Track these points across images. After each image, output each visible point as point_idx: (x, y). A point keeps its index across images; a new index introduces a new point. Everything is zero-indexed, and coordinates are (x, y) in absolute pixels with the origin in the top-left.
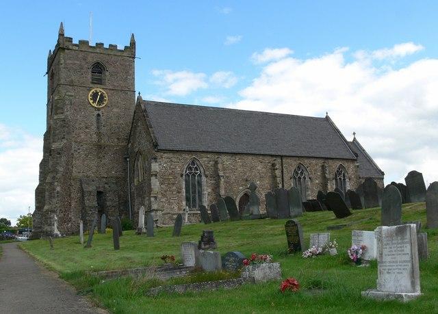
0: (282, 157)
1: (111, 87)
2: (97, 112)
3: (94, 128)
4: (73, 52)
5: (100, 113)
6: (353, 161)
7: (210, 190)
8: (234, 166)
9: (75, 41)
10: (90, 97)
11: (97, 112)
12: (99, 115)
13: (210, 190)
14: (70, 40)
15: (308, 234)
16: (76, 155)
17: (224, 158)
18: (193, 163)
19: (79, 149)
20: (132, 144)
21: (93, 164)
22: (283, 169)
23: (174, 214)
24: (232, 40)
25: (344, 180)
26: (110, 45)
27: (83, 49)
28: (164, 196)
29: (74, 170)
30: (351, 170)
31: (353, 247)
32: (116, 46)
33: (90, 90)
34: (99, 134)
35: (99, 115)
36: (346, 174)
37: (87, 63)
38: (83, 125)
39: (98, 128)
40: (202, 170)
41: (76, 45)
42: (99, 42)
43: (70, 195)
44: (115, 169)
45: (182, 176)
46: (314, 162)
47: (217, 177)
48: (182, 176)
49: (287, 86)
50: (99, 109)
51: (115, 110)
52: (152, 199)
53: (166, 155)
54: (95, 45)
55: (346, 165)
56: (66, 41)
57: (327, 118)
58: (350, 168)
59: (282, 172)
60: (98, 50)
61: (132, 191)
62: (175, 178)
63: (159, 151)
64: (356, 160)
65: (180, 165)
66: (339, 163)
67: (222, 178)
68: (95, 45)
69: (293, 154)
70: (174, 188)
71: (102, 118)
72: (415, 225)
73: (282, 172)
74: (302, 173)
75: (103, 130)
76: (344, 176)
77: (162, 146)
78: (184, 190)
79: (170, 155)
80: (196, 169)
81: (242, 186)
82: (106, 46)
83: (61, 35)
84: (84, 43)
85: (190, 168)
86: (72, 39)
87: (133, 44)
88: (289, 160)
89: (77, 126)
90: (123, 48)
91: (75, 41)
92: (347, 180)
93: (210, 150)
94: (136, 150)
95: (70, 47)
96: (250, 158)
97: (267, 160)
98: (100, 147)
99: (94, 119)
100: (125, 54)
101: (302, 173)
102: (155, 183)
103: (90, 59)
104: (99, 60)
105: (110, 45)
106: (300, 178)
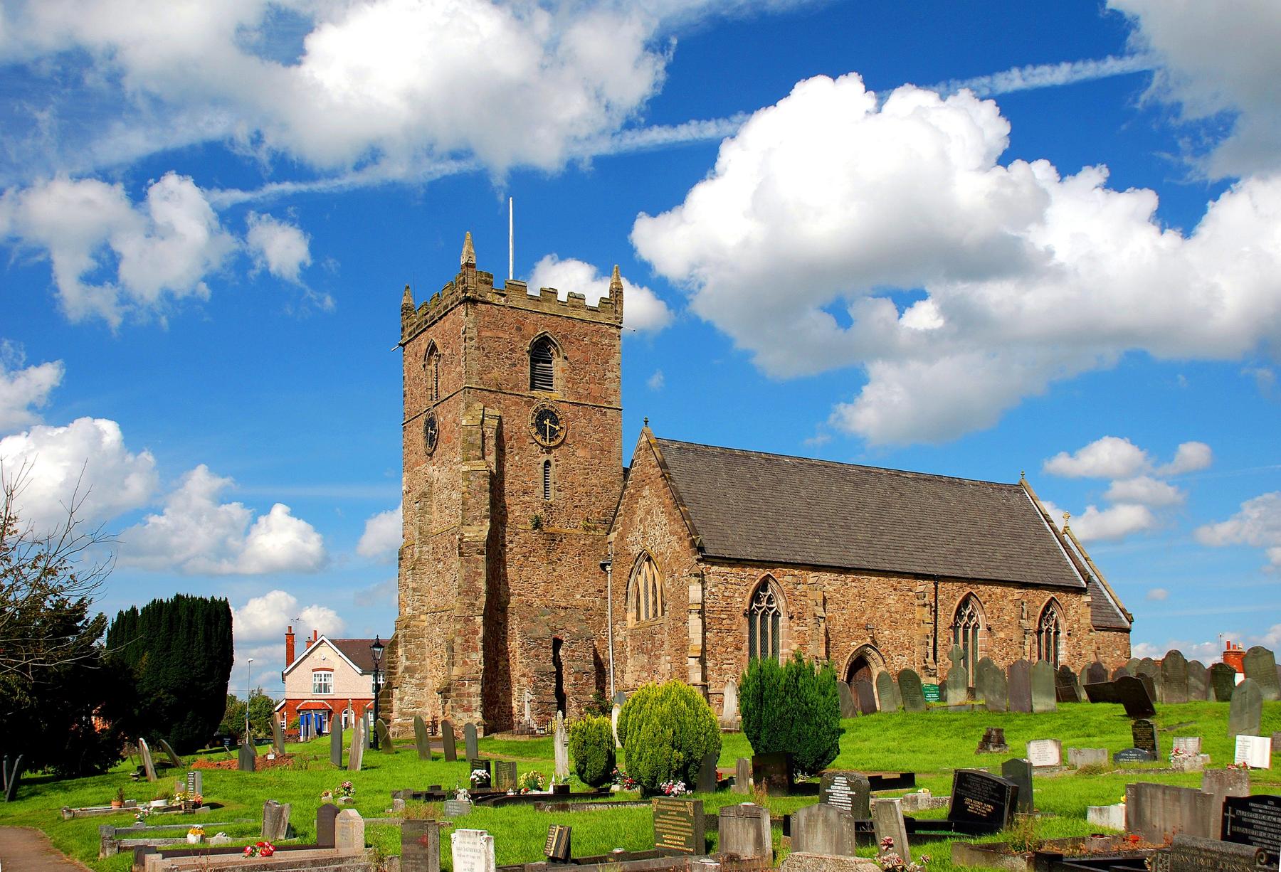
2: (545, 457)
5: (551, 457)
11: (545, 457)
15: (396, 719)
20: (622, 537)
24: (1159, 593)
25: (1057, 633)
27: (514, 304)
31: (800, 775)
35: (547, 463)
42: (547, 287)
49: (1047, 507)
51: (580, 453)
53: (714, 569)
59: (936, 611)
61: (618, 639)
69: (959, 573)
76: (1056, 625)
78: (747, 644)
82: (562, 297)
88: (949, 586)
93: (799, 559)
94: (636, 550)
95: (489, 297)
100: (602, 318)
103: (529, 329)
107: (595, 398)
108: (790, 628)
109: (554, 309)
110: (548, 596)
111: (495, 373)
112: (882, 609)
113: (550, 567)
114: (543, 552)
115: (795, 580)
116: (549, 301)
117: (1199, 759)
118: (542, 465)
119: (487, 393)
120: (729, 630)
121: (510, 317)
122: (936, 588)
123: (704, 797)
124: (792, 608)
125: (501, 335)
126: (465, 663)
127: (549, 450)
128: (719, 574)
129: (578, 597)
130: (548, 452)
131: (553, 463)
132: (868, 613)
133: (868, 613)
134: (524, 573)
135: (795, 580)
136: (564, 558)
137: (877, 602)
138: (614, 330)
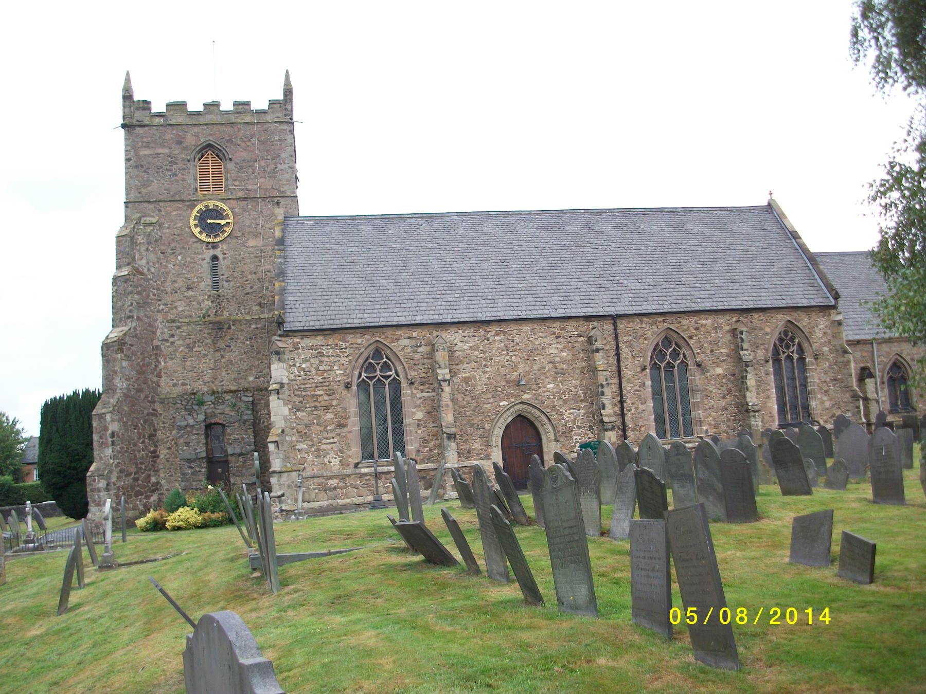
0: (614, 318)
1: (240, 194)
2: (212, 252)
3: (206, 283)
4: (153, 131)
5: (218, 252)
6: (825, 309)
7: (420, 415)
8: (484, 352)
9: (158, 107)
10: (193, 222)
11: (212, 252)
12: (215, 258)
13: (420, 415)
14: (146, 105)
16: (165, 348)
17: (456, 337)
18: (377, 354)
19: (173, 336)
21: (205, 366)
22: (618, 349)
23: (331, 478)
25: (802, 359)
26: (236, 104)
28: (304, 436)
29: (164, 380)
30: (818, 333)
32: (247, 104)
33: (193, 207)
34: (217, 299)
35: (215, 258)
36: (805, 345)
37: (185, 148)
38: (180, 283)
39: (215, 285)
40: (399, 368)
41: (160, 115)
42: (209, 101)
43: (151, 437)
44: (254, 372)
45: (348, 386)
46: (709, 322)
47: (432, 383)
48: (348, 386)
50: (214, 246)
52: (271, 447)
53: (307, 342)
54: (201, 109)
55: (804, 321)
56: (137, 109)
57: (770, 208)
58: (818, 330)
59: (618, 355)
60: (208, 118)
62: (331, 393)
63: (287, 334)
64: (834, 307)
65: (341, 363)
66: (780, 320)
67: (444, 384)
68: (201, 109)
70: (329, 416)
71: (223, 264)
72: (828, 619)
73: (618, 355)
74: (675, 354)
75: (226, 289)
76: (801, 350)
77: (296, 319)
79: (319, 340)
80: (386, 367)
81: (507, 397)
83: (128, 97)
84: (178, 107)
85: (370, 368)
86: (148, 103)
87: (288, 92)
88: (636, 325)
89: (168, 287)
90: (265, 106)
91: (158, 107)
92: (809, 359)
96: (527, 328)
97: (572, 329)
98: (219, 328)
99: (206, 266)
101: (675, 354)
102: (279, 411)
103: (190, 140)
104: (211, 139)
105: (236, 104)
106: (670, 366)
107: (266, 190)
108: (413, 395)
109: (219, 119)
110: (217, 383)
111: (154, 186)
112: (541, 361)
113: (218, 355)
114: (209, 341)
115: (413, 342)
116: (211, 113)
117: (787, 577)
118: (208, 260)
119: (146, 205)
120: (327, 408)
121: (169, 135)
122: (615, 330)
123: (822, 496)
124: (413, 374)
125: (160, 151)
126: (101, 458)
127: (214, 246)
128: (311, 348)
129: (251, 379)
130: (214, 248)
131: (221, 256)
132: (522, 368)
133: (522, 368)
134: (188, 363)
135: (413, 342)
136: (233, 344)
137: (531, 354)
138: (285, 127)
